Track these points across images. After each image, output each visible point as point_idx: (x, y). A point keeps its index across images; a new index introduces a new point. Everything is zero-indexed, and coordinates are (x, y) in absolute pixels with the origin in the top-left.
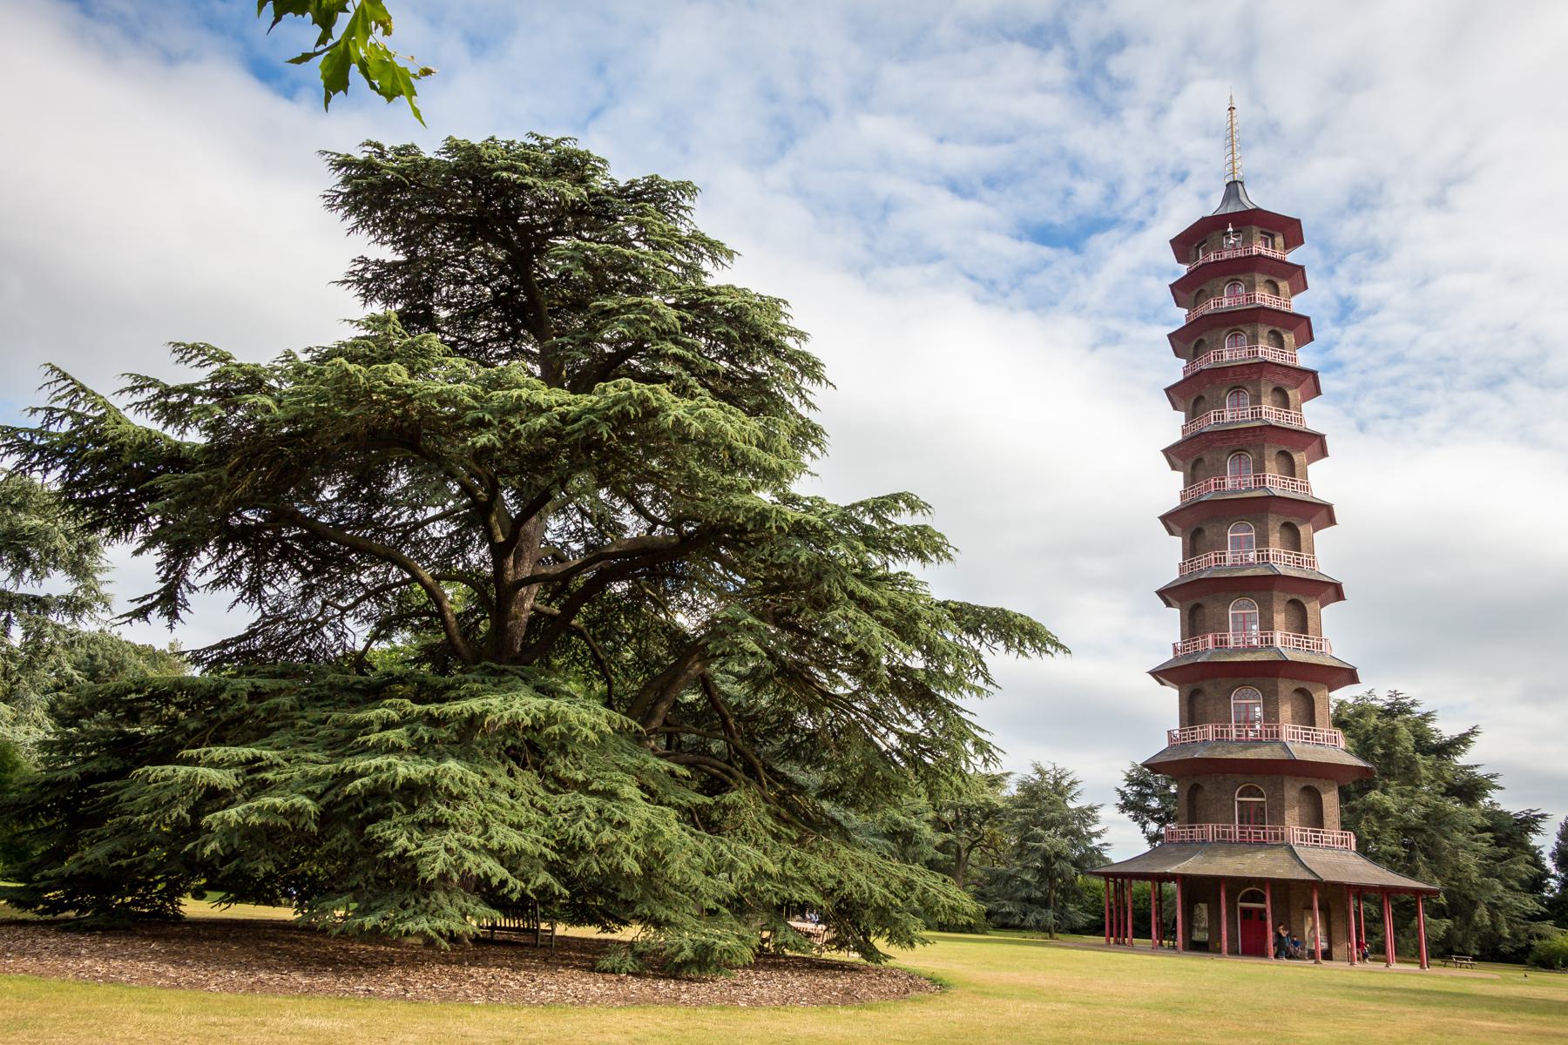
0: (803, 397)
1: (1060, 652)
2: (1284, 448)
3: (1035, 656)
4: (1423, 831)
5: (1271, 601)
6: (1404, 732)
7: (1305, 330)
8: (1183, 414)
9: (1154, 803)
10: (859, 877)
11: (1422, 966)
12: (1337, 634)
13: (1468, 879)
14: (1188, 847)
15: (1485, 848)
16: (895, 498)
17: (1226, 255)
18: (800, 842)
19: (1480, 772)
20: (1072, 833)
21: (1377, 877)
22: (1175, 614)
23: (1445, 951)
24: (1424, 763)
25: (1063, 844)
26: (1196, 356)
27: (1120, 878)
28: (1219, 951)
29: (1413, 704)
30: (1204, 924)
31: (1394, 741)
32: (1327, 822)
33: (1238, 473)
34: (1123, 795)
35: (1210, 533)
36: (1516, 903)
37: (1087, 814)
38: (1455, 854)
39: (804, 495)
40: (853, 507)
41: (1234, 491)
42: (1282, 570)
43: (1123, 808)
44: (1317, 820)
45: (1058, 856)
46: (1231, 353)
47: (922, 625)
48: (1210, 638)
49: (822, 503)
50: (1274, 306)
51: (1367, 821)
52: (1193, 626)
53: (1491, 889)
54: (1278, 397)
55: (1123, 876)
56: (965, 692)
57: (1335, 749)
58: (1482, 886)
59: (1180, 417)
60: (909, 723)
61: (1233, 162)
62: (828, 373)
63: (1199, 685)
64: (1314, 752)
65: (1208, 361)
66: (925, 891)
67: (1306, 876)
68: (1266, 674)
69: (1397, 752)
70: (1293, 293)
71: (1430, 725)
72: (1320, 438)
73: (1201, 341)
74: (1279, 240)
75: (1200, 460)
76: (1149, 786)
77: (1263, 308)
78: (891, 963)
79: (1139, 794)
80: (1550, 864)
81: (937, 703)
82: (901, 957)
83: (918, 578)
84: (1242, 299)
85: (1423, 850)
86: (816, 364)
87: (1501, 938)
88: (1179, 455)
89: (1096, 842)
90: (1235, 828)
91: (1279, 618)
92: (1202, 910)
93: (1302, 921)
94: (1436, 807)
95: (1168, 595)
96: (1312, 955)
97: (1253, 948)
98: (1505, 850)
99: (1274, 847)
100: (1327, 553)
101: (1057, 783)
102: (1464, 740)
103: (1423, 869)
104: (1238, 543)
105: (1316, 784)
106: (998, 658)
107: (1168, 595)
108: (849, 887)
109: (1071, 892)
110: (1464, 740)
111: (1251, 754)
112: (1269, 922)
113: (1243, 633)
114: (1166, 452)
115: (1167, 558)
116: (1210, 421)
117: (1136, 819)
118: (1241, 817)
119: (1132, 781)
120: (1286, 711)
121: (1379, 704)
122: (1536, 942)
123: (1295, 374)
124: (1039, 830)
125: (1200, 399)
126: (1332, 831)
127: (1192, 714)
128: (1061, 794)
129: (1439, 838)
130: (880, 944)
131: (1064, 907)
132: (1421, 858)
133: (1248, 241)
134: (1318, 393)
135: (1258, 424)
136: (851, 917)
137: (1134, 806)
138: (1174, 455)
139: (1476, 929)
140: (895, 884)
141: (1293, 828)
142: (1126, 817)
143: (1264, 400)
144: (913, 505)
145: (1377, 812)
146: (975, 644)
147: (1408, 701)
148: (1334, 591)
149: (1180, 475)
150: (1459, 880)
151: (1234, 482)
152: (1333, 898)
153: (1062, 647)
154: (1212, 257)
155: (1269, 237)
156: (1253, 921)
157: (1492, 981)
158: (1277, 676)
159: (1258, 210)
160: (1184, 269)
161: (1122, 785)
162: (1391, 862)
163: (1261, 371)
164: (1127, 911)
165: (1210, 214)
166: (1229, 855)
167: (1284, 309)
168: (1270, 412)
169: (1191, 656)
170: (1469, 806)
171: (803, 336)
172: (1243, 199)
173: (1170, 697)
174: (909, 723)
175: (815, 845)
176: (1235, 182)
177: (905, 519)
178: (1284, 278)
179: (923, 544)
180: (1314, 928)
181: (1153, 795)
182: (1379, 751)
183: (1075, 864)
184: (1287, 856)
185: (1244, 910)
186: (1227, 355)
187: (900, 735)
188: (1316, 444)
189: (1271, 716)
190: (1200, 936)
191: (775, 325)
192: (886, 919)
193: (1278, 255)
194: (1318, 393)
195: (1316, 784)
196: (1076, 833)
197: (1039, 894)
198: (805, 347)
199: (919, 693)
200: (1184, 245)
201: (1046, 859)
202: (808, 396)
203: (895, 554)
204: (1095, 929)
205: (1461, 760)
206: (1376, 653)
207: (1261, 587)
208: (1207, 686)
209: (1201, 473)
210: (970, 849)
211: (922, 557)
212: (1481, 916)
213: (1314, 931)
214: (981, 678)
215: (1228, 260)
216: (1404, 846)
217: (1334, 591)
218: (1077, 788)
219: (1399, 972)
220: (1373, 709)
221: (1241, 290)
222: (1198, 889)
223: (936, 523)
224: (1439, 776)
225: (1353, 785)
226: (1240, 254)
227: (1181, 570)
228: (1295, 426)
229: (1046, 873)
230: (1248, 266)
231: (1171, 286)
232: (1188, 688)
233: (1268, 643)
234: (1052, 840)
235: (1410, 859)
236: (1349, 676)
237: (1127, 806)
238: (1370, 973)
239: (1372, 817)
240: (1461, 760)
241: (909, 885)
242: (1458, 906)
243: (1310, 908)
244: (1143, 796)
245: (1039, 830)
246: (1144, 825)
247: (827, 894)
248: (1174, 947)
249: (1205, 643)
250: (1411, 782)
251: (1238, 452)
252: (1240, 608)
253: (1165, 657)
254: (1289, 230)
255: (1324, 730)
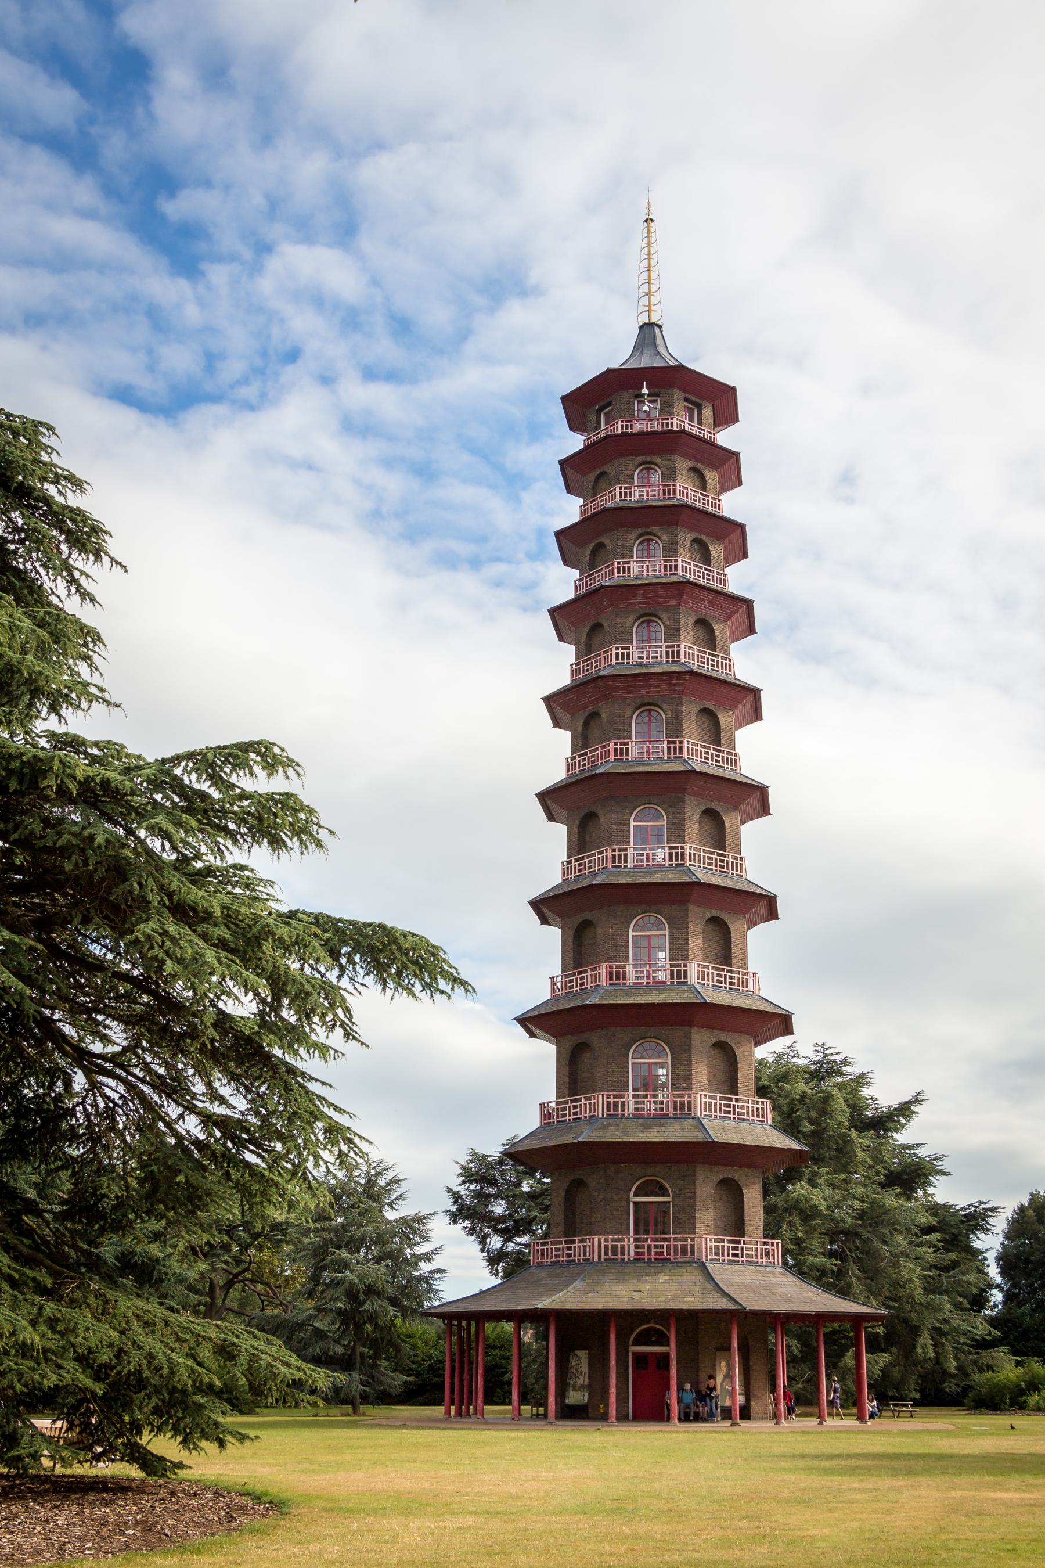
0: (73, 581)
1: (459, 990)
2: (708, 704)
3: (425, 996)
4: (857, 1234)
5: (685, 919)
6: (840, 1103)
7: (738, 542)
8: (572, 649)
9: (499, 1208)
10: (149, 1342)
11: (821, 1417)
12: (769, 964)
13: (911, 1297)
14: (567, 1269)
15: (928, 1254)
16: (245, 747)
17: (638, 427)
18: (50, 1294)
19: (922, 1152)
20: (389, 1255)
21: (812, 1302)
22: (554, 934)
23: (888, 1394)
24: (861, 1141)
25: (379, 1273)
26: (592, 566)
27: (464, 1320)
28: (604, 1417)
29: (845, 1062)
30: (583, 1380)
31: (824, 1112)
32: (749, 1228)
33: (646, 737)
34: (456, 1197)
35: (606, 819)
36: (965, 1327)
37: (413, 1228)
38: (896, 1265)
39: (91, 738)
40: (177, 759)
41: (640, 762)
42: (702, 876)
43: (455, 1217)
44: (736, 1227)
45: (372, 1291)
46: (642, 566)
47: (267, 946)
48: (603, 970)
49: (119, 751)
50: (699, 505)
51: (791, 1224)
52: (578, 953)
53: (938, 1309)
54: (701, 633)
55: (469, 1316)
56: (302, 1051)
57: (757, 1128)
58: (927, 1306)
59: (569, 652)
60: (223, 1101)
61: (649, 294)
62: (112, 546)
63: (584, 1037)
64: (736, 1130)
65: (609, 576)
66: (254, 1358)
67: (723, 1304)
68: (676, 1020)
69: (834, 1128)
70: (724, 489)
71: (865, 1092)
72: (754, 693)
73: (601, 545)
74: (708, 413)
75: (594, 715)
76: (493, 1183)
77: (686, 506)
78: (183, 1474)
79: (479, 1195)
80: (993, 1272)
81: (274, 1068)
82: (207, 1465)
83: (261, 875)
84: (658, 491)
85: (858, 1261)
86: (96, 530)
87: (945, 1373)
88: (567, 707)
89: (425, 1267)
90: (629, 1243)
91: (696, 943)
92: (581, 1361)
93: (714, 1367)
94: (873, 1202)
95: (545, 907)
96: (727, 1414)
97: (649, 1410)
98: (953, 1256)
99: (680, 1264)
100: (760, 852)
101: (371, 1183)
102: (905, 1110)
103: (857, 1287)
104: (643, 835)
105: (736, 1174)
106: (368, 999)
107: (545, 907)
108: (135, 1360)
109: (385, 1342)
110: (905, 1110)
111: (654, 1136)
112: (674, 1372)
113: (650, 963)
114: (564, 399)
115: (546, 854)
116: (611, 661)
117: (472, 1231)
118: (636, 1224)
119: (468, 1176)
120: (701, 1072)
121: (801, 1062)
122: (977, 1377)
123: (726, 603)
124: (343, 1254)
125: (597, 627)
126: (754, 1240)
127: (573, 1079)
128: (377, 1198)
129: (876, 1243)
130: (164, 1445)
131: (375, 1366)
132: (854, 1270)
133: (667, 410)
134: (752, 631)
135: (674, 668)
136: (117, 1404)
137: (469, 1213)
138: (561, 705)
139: (915, 1363)
140: (206, 1353)
141: (707, 1240)
142: (458, 1230)
143: (683, 634)
144: (271, 759)
145: (802, 1211)
146: (332, 976)
147: (839, 1058)
148: (765, 906)
149: (565, 737)
150: (899, 1299)
151: (642, 748)
152: (753, 1330)
153: (463, 983)
154: (619, 428)
155: (694, 406)
156: (650, 1374)
157: (949, 1434)
158: (690, 1025)
159: (681, 368)
160: (576, 442)
161: (455, 1182)
162: (819, 1277)
163: (680, 595)
164: (463, 1370)
165: (616, 365)
166: (621, 1279)
167: (711, 509)
168: (691, 654)
169: (575, 995)
170: (909, 1198)
171: (78, 484)
172: (661, 349)
173: (544, 1052)
174: (223, 1101)
175: (77, 1295)
176: (651, 325)
177: (257, 782)
178: (713, 466)
179: (278, 821)
180: (729, 1376)
181: (496, 1196)
182: (808, 1127)
183: (394, 1302)
184: (698, 1277)
185: (639, 1358)
186: (635, 569)
187: (208, 1120)
188: (747, 701)
189: (681, 1080)
190: (576, 1397)
191: (37, 461)
192: (185, 1411)
193: (705, 434)
194: (752, 631)
195: (736, 1174)
196: (395, 1256)
197: (340, 1349)
198: (74, 500)
199: (244, 1053)
200: (584, 404)
201: (352, 1295)
202: (83, 581)
203: (232, 835)
204: (412, 1396)
205: (901, 1138)
206: (822, 998)
207: (671, 898)
208: (596, 1039)
209: (595, 732)
210: (229, 1285)
211: (276, 843)
212: (924, 1347)
213: (727, 1382)
214: (339, 1032)
215: (640, 434)
216: (832, 1254)
217: (765, 906)
218: (399, 1190)
219: (838, 1431)
220: (799, 1070)
221: (657, 477)
222: (579, 1331)
223: (306, 790)
224: (878, 1159)
225: (780, 1170)
226: (657, 426)
227: (569, 767)
228: (722, 674)
229: (351, 1319)
230: (661, 446)
231: (562, 463)
232: (570, 1042)
233: (681, 977)
234: (362, 1266)
235: (840, 1274)
236: (781, 1023)
237: (461, 1212)
238: (800, 1434)
239: (797, 1220)
240: (901, 1138)
241: (226, 1352)
242: (897, 1333)
243: (728, 1349)
244: (481, 1197)
245: (343, 1254)
246: (483, 1240)
247: (100, 1373)
248: (545, 1416)
249: (596, 978)
250: (844, 1169)
251: (648, 706)
252: (643, 928)
253: (537, 993)
254: (720, 400)
255: (748, 1100)
